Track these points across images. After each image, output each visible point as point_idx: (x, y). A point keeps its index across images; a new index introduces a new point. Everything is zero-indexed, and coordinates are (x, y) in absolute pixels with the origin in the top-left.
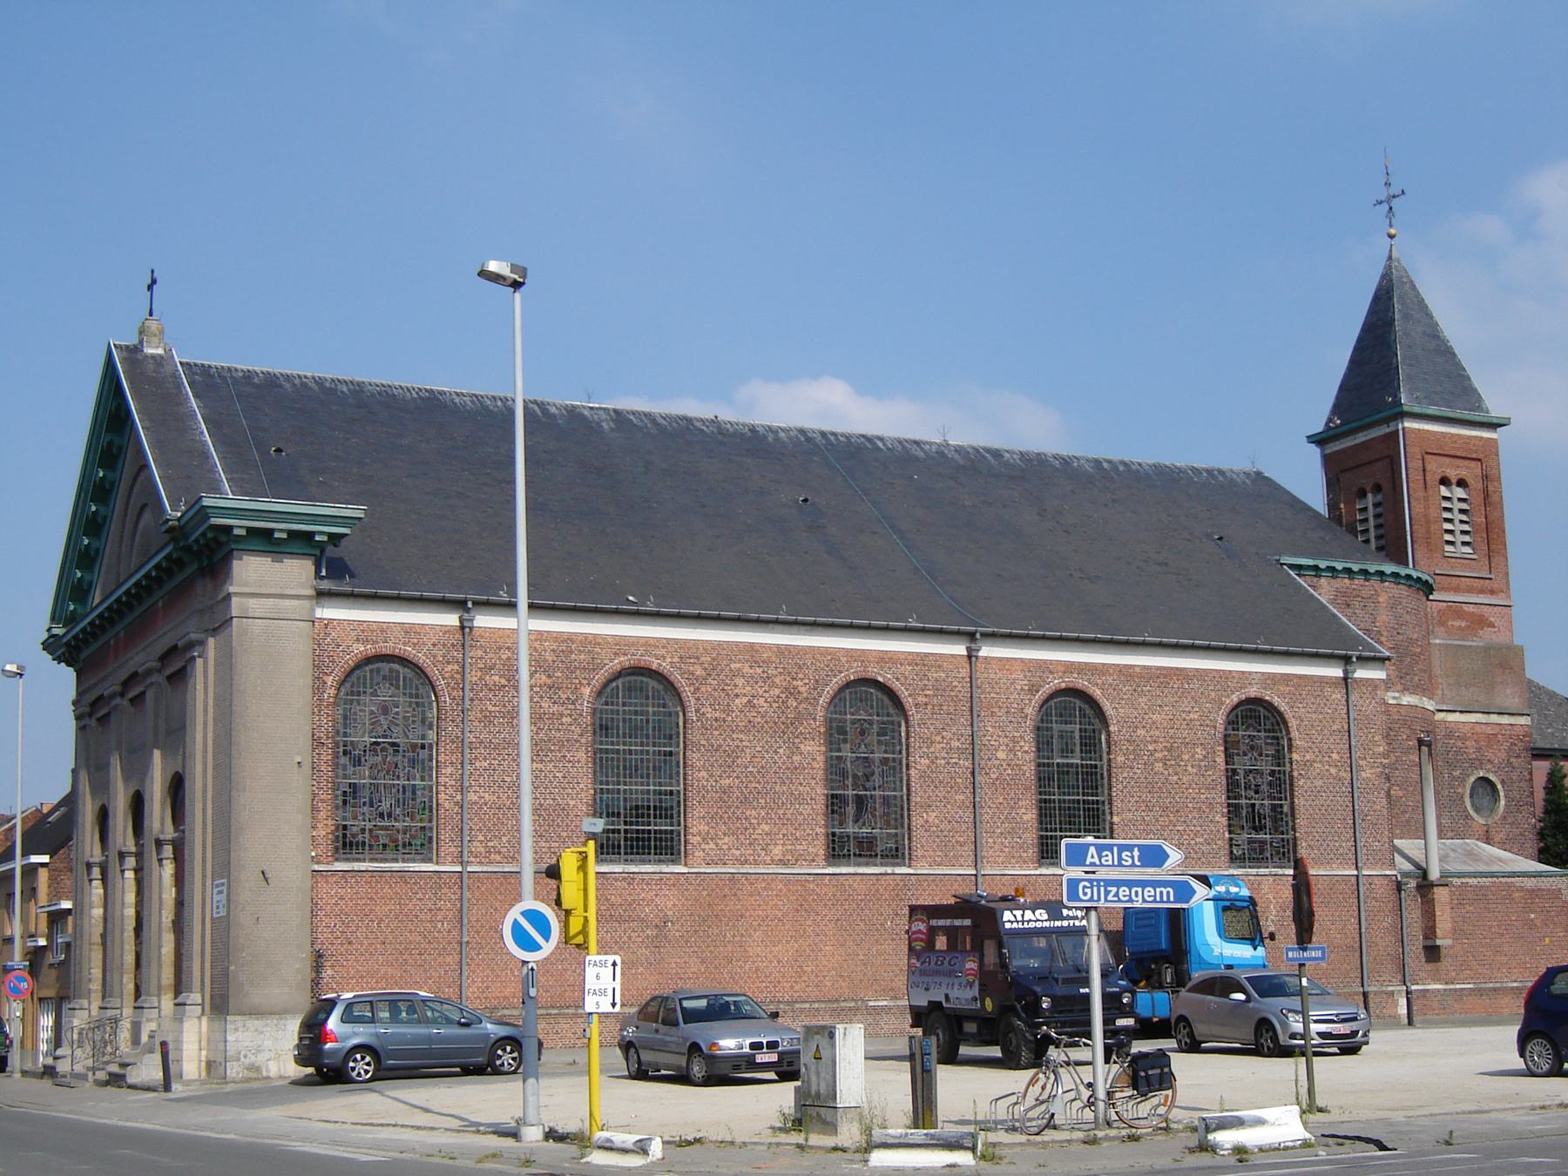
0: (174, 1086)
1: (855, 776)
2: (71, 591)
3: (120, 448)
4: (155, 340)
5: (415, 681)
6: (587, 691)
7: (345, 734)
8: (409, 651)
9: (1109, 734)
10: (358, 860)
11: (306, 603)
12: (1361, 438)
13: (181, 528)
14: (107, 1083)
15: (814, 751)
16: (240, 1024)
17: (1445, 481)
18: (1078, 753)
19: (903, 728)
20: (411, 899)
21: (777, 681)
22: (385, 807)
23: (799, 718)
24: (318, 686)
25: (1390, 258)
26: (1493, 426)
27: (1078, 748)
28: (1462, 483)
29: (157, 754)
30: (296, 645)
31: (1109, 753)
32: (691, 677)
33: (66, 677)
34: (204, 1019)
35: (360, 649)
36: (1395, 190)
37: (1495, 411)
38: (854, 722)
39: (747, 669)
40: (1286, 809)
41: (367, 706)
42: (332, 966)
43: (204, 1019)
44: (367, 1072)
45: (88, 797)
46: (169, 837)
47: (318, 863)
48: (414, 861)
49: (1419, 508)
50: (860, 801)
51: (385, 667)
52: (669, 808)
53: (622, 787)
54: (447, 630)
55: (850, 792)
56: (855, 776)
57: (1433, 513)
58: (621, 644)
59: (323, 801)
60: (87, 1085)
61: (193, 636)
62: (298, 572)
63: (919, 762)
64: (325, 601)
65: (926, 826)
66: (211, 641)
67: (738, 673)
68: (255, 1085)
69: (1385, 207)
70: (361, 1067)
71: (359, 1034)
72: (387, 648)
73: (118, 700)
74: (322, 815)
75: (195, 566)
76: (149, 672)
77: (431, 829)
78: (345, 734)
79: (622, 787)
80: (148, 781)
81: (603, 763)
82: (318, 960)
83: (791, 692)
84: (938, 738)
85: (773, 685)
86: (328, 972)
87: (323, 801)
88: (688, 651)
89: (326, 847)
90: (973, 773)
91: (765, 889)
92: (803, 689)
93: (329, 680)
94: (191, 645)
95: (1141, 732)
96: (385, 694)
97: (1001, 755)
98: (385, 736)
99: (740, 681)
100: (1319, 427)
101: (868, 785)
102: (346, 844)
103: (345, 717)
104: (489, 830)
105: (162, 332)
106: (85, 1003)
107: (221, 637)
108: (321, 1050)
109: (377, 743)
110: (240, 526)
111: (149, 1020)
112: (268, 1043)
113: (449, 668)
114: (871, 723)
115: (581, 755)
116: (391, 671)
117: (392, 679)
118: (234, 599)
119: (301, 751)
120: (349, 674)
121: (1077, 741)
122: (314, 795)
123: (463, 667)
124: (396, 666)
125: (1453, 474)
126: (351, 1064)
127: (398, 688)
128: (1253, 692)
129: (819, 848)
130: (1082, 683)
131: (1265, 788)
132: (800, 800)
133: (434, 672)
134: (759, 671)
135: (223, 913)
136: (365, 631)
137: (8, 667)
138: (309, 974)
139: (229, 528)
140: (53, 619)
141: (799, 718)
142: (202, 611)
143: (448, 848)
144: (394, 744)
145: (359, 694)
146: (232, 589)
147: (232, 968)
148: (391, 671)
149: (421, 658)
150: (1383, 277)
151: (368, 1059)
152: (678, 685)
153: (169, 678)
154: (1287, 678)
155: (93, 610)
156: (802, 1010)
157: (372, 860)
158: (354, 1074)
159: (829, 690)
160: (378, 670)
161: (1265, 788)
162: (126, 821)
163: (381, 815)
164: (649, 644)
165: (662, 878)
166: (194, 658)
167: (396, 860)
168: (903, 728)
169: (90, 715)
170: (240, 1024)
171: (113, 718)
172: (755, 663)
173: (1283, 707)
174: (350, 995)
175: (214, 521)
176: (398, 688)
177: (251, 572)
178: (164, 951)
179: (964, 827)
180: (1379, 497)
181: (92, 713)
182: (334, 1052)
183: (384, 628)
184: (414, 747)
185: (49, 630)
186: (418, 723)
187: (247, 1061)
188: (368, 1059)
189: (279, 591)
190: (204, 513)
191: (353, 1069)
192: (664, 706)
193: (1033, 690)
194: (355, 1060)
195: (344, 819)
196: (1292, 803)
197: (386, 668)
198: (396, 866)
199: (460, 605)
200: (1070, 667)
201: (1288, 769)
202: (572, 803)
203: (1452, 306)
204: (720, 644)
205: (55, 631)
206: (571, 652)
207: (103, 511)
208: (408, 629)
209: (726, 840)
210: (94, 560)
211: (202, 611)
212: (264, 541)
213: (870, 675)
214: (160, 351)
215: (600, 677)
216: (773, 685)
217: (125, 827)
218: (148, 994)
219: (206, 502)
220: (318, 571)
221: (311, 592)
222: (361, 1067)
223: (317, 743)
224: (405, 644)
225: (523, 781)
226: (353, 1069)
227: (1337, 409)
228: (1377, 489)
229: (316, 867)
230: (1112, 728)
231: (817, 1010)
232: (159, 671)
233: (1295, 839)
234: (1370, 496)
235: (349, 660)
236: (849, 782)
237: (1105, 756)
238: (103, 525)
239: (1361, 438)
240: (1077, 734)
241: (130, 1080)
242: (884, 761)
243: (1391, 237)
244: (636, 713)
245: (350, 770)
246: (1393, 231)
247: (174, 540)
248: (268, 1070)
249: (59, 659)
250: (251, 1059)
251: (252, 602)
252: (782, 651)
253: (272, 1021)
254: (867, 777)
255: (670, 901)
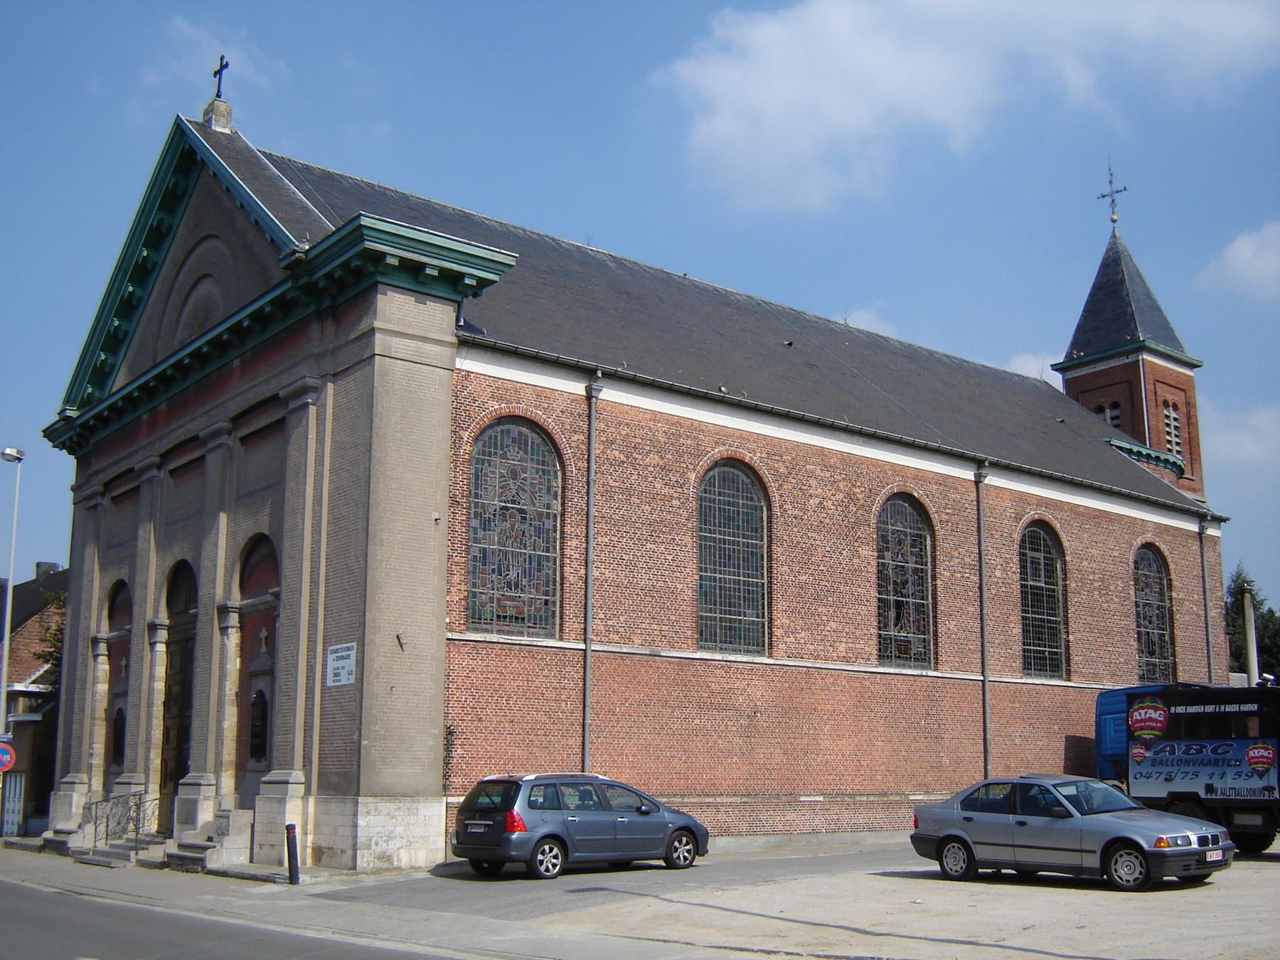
0: (302, 877)
1: (895, 582)
2: (92, 371)
3: (170, 227)
4: (223, 120)
5: (542, 448)
6: (692, 476)
7: (476, 496)
8: (539, 415)
9: (1064, 563)
10: (486, 631)
11: (447, 351)
12: (1100, 367)
13: (308, 262)
14: (162, 866)
15: (868, 552)
16: (372, 807)
17: (1166, 404)
18: (1043, 578)
19: (928, 542)
20: (537, 676)
21: (841, 485)
22: (512, 575)
23: (857, 524)
24: (456, 442)
25: (1114, 236)
26: (1192, 366)
27: (1043, 573)
28: (1175, 407)
29: (223, 517)
30: (433, 391)
31: (1065, 579)
32: (776, 474)
33: (65, 465)
34: (312, 801)
35: (495, 407)
36: (1117, 186)
37: (1191, 354)
38: (894, 532)
39: (818, 472)
40: (1167, 638)
41: (497, 469)
42: (463, 745)
43: (312, 801)
44: (554, 866)
45: (97, 574)
46: (237, 604)
47: (451, 630)
48: (538, 635)
49: (1153, 422)
50: (899, 605)
51: (515, 429)
52: (761, 599)
53: (718, 575)
54: (573, 398)
55: (892, 598)
56: (895, 582)
57: (1161, 426)
58: (722, 434)
59: (457, 564)
60: (129, 865)
61: (310, 381)
62: (437, 317)
63: (944, 574)
64: (464, 351)
65: (949, 633)
66: (330, 386)
67: (811, 475)
68: (389, 877)
69: (1108, 200)
70: (550, 859)
71: (548, 822)
72: (521, 409)
73: (154, 472)
74: (456, 579)
75: (313, 308)
76: (217, 434)
77: (554, 603)
78: (476, 496)
79: (718, 575)
80: (207, 545)
81: (706, 552)
82: (449, 733)
83: (851, 497)
84: (956, 554)
85: (838, 489)
86: (458, 751)
87: (457, 564)
88: (775, 448)
89: (458, 615)
90: (980, 588)
91: (833, 684)
92: (860, 496)
93: (465, 435)
94: (305, 390)
95: (1085, 563)
96: (515, 457)
97: (998, 573)
98: (513, 502)
99: (813, 483)
100: (1060, 359)
101: (904, 591)
102: (475, 616)
103: (477, 477)
104: (609, 609)
105: (230, 113)
106: (85, 777)
107: (350, 381)
108: (509, 840)
109: (506, 509)
110: (394, 254)
111: (207, 798)
112: (400, 829)
113: (575, 438)
114: (905, 534)
115: (688, 540)
116: (520, 433)
117: (521, 442)
118: (378, 335)
119: (438, 506)
120: (483, 432)
121: (1042, 567)
122: (450, 557)
123: (589, 438)
124: (524, 430)
125: (1170, 398)
126: (540, 857)
127: (526, 453)
128: (1149, 537)
129: (872, 648)
130: (1048, 517)
131: (1154, 619)
132: (858, 600)
133: (561, 440)
134: (828, 475)
135: (347, 679)
136: (501, 389)
137: (8, 451)
138: (442, 754)
139: (383, 255)
140: (67, 401)
141: (857, 524)
142: (319, 356)
143: (573, 625)
144: (521, 511)
145: (490, 454)
146: (377, 324)
147: (364, 743)
148: (520, 433)
149: (551, 425)
150: (1108, 250)
151: (556, 851)
152: (766, 480)
153: (243, 440)
154: (1168, 528)
155: (111, 396)
156: (861, 803)
157: (499, 632)
158: (542, 868)
159: (880, 500)
160: (509, 431)
161: (1154, 619)
162: (158, 589)
163: (509, 585)
164: (743, 436)
165: (752, 669)
166: (306, 405)
167: (521, 633)
168: (928, 542)
169: (103, 495)
170: (372, 807)
171: (144, 492)
172: (825, 467)
173: (1166, 553)
174: (532, 777)
175: (368, 244)
176: (526, 453)
177: (395, 309)
178: (226, 724)
179: (974, 635)
180: (1116, 413)
181: (86, 498)
182: (522, 843)
183: (518, 387)
184: (540, 515)
185: (63, 411)
186: (544, 491)
187: (378, 850)
188: (556, 851)
189: (422, 334)
190: (358, 233)
191: (541, 862)
192: (752, 500)
193: (1018, 518)
194: (543, 853)
195: (474, 585)
196: (1172, 633)
197: (518, 431)
198: (525, 640)
199: (588, 373)
200: (1042, 502)
201: (1167, 605)
202: (680, 587)
203: (1162, 279)
204: (799, 445)
205: (69, 413)
206: (680, 436)
207: (139, 292)
208: (540, 392)
209: (803, 634)
210: (121, 342)
211: (319, 356)
212: (414, 276)
213: (908, 490)
214: (227, 131)
215: (704, 463)
216: (838, 489)
217: (157, 601)
218: (78, 771)
219: (365, 221)
220: (458, 320)
221: (454, 340)
222: (550, 859)
223: (454, 502)
224: (536, 408)
225: (638, 562)
226: (541, 862)
227: (1075, 344)
228: (1115, 406)
229: (450, 635)
230: (1068, 558)
231: (872, 803)
232: (229, 433)
233: (1175, 663)
234: (1108, 411)
235: (484, 417)
236: (891, 588)
237: (1060, 583)
238: (136, 307)
239: (1100, 367)
240: (1042, 561)
241: (211, 865)
242: (916, 571)
243: (1114, 221)
244: (729, 504)
245: (481, 534)
246: (1115, 217)
247: (294, 277)
248: (399, 860)
249: (61, 446)
250: (383, 846)
251: (395, 341)
252: (846, 458)
253: (405, 804)
254: (905, 583)
255: (758, 691)
